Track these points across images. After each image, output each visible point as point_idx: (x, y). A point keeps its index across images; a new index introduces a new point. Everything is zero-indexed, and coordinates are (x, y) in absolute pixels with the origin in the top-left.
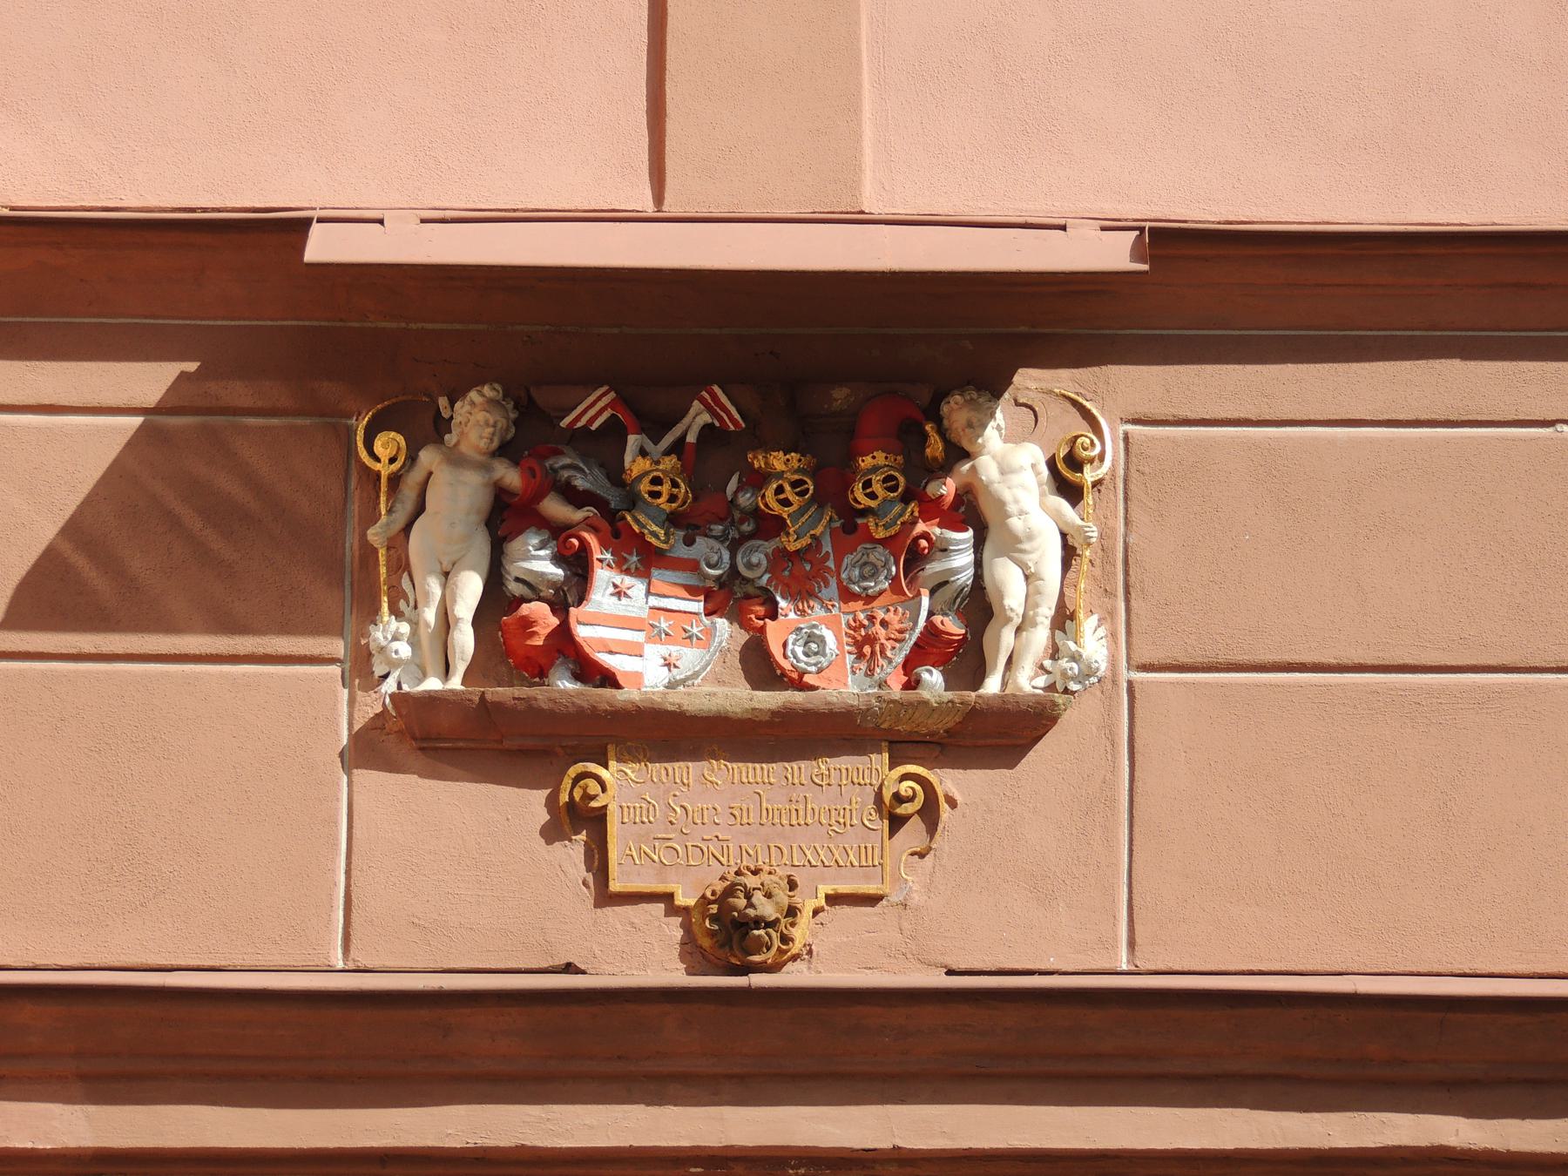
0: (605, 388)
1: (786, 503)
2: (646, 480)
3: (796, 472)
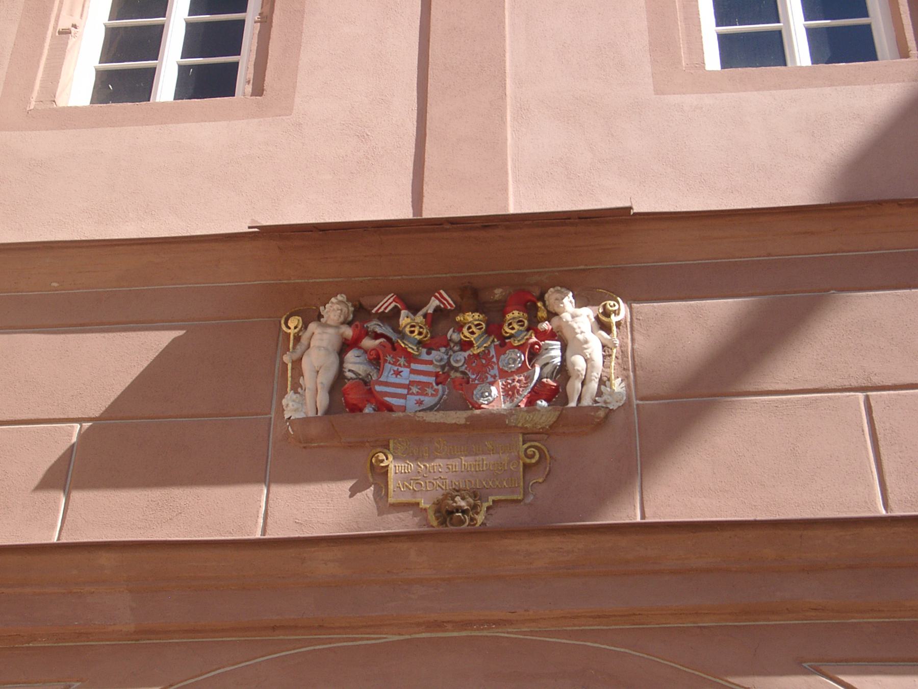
0: (392, 294)
1: (473, 333)
2: (409, 326)
3: (478, 320)
